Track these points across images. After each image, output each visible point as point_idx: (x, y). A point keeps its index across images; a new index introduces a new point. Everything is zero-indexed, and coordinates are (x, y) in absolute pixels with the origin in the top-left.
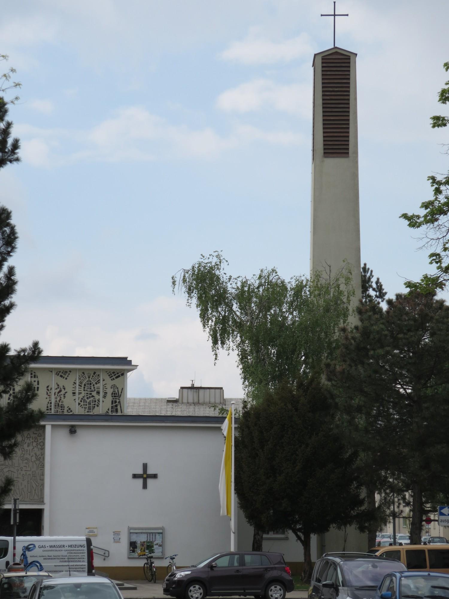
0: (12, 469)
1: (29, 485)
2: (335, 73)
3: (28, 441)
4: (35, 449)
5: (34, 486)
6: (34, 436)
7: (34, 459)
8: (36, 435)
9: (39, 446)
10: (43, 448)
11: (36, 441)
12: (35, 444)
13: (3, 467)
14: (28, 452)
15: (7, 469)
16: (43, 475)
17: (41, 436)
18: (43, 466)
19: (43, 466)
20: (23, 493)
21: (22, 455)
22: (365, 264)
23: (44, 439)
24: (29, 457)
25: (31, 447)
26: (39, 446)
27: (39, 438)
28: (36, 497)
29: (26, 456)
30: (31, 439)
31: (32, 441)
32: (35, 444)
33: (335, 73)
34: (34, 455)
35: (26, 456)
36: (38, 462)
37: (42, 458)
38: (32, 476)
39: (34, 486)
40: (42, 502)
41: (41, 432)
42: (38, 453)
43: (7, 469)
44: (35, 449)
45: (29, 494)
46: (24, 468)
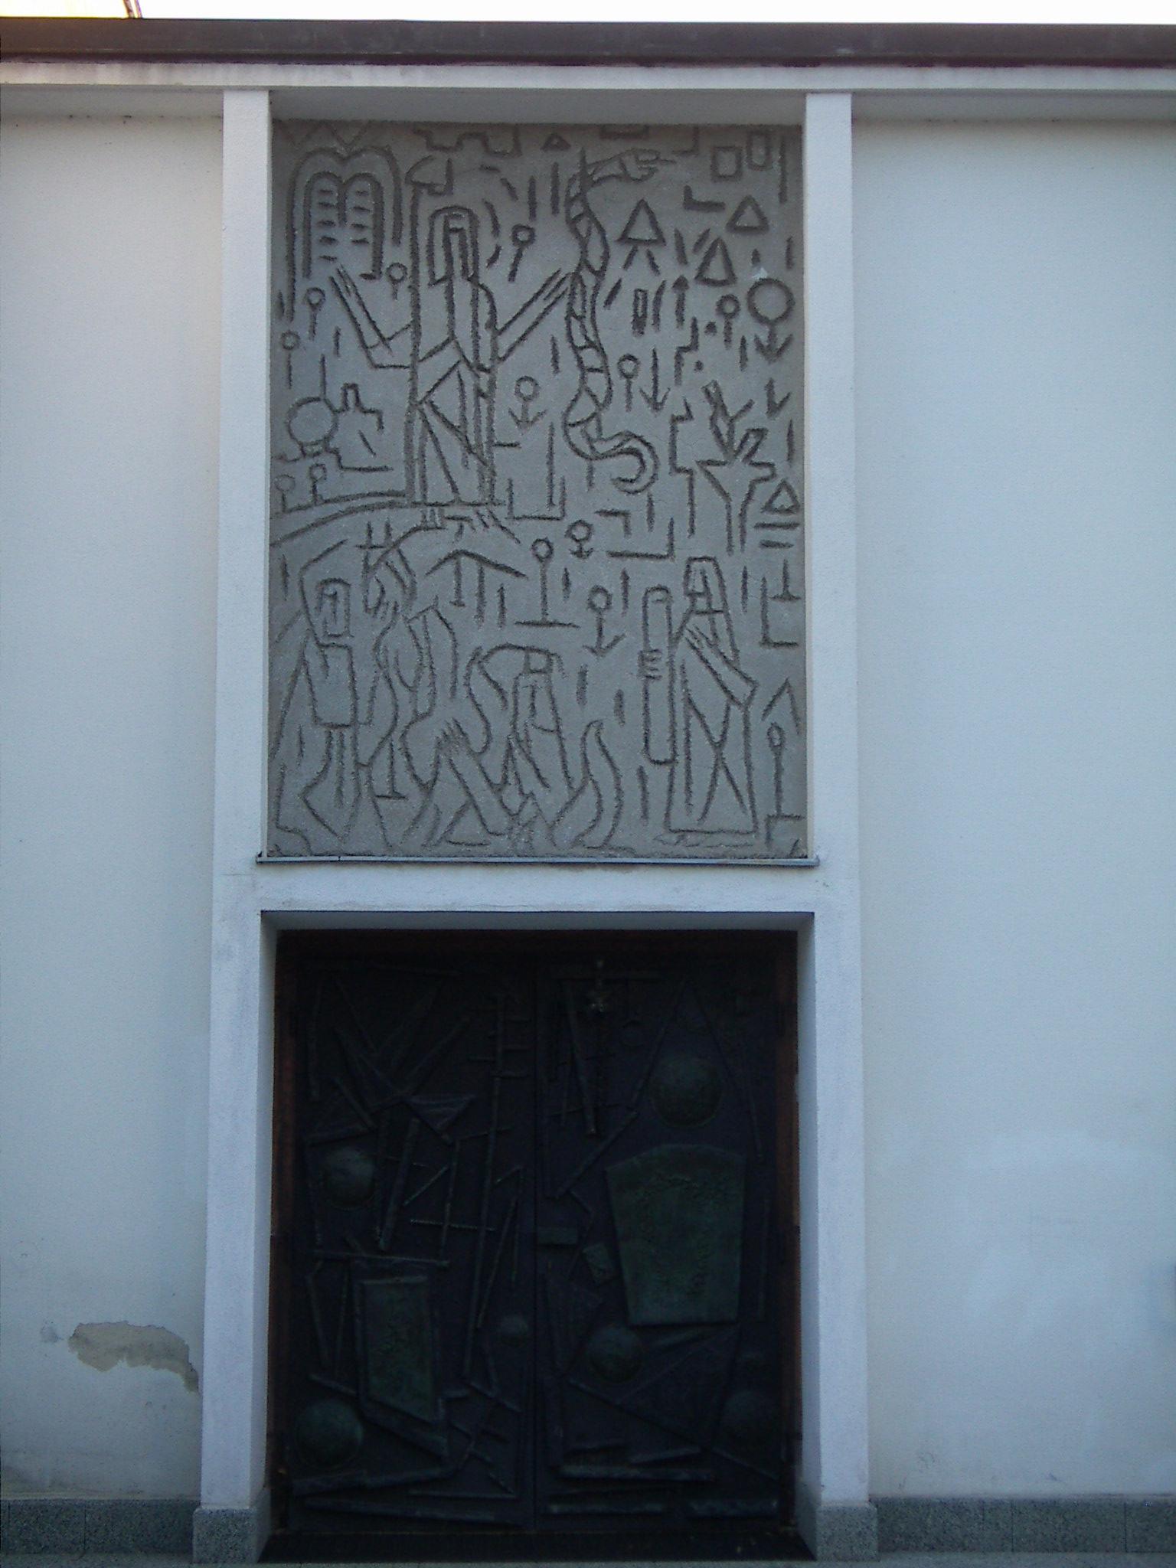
0: (487, 542)
1: (658, 689)
2: (620, 696)
3: (639, 277)
4: (710, 346)
5: (710, 699)
6: (693, 225)
7: (697, 442)
8: (717, 224)
9: (745, 326)
10: (781, 341)
11: (716, 271)
12: (702, 303)
13: (410, 517)
14: (643, 380)
15: (441, 544)
16: (792, 594)
17: (762, 227)
18: (788, 509)
19: (786, 511)
20: (599, 766)
21: (585, 407)
22: (395, 295)
23: (793, 254)
24: (654, 428)
25: (668, 336)
26: (745, 326)
27: (739, 248)
28: (727, 812)
29: (616, 419)
30: (666, 258)
31: (671, 271)
32: (702, 303)
33: (620, 696)
34: (703, 410)
35: (616, 419)
36: (737, 476)
37: (776, 438)
38: (681, 604)
39: (710, 699)
40: (796, 858)
41: (762, 187)
42: (741, 387)
43: (441, 544)
44: (710, 346)
45: (658, 777)
46: (607, 535)
